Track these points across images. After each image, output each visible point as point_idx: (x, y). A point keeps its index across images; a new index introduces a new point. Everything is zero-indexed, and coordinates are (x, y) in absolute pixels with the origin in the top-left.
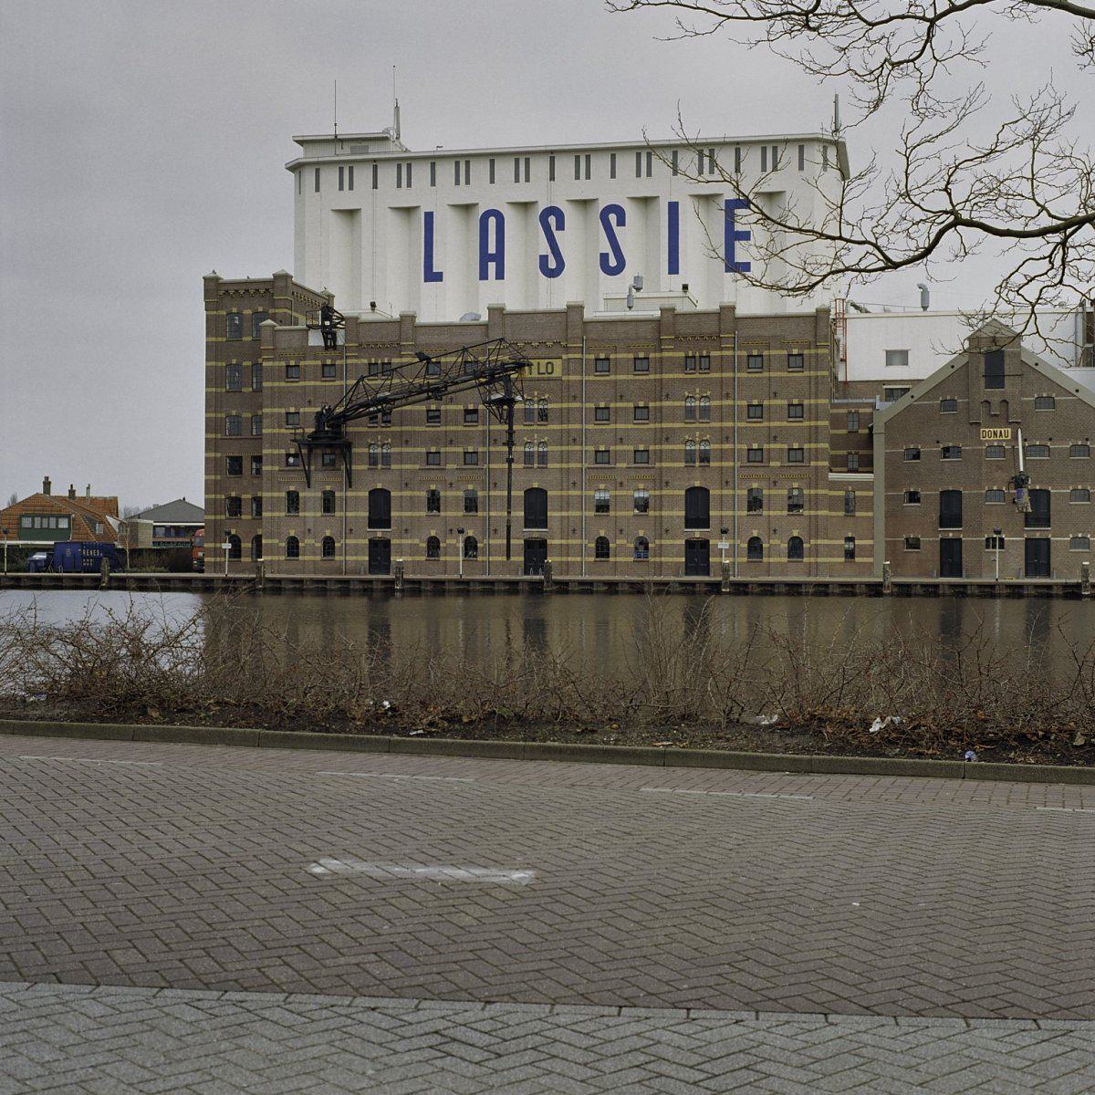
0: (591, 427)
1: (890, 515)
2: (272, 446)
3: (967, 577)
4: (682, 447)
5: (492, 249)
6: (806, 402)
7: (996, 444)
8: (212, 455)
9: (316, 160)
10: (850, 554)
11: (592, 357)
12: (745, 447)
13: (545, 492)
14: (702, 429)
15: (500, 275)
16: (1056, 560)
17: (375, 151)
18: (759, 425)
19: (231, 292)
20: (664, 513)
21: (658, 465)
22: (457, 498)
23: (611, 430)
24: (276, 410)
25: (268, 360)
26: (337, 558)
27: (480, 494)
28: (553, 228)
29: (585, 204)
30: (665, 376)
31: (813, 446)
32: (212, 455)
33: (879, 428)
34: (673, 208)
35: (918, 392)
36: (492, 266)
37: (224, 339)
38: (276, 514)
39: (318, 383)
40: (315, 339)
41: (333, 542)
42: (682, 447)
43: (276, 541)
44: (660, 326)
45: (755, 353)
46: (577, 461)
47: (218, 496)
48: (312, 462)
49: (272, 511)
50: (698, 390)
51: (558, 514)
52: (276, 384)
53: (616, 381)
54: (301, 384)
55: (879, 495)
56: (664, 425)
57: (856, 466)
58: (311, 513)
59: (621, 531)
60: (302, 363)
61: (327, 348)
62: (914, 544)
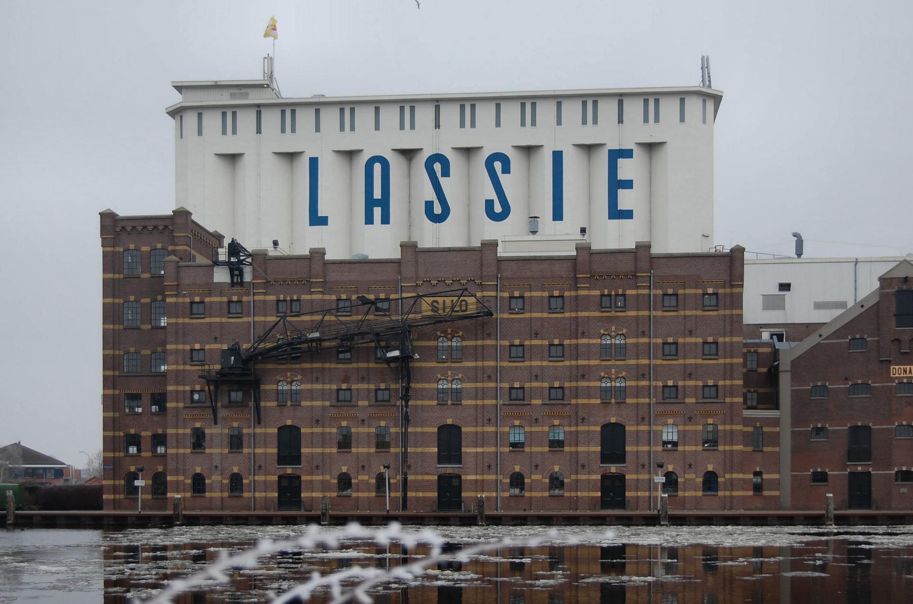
0: (505, 364)
1: (796, 450)
2: (177, 383)
3: (877, 509)
4: (598, 384)
5: (377, 194)
6: (721, 340)
7: (905, 381)
8: (110, 392)
9: (199, 104)
10: (758, 488)
11: (506, 295)
12: (660, 384)
13: (458, 429)
14: (617, 366)
15: (385, 220)
16: (877, 491)
17: (255, 97)
18: (674, 362)
19: (129, 229)
20: (580, 449)
21: (573, 401)
22: (696, 432)
23: (526, 367)
24: (181, 347)
25: (172, 296)
26: (246, 495)
27: (245, 431)
28: (439, 174)
29: (468, 152)
30: (581, 314)
31: (728, 382)
32: (110, 392)
33: (785, 363)
34: (558, 157)
35: (826, 332)
36: (377, 211)
37: (122, 276)
38: (181, 451)
39: (224, 320)
40: (221, 276)
41: (204, 479)
42: (598, 384)
43: (181, 478)
44: (575, 264)
45: (670, 291)
46: (491, 398)
47: (117, 434)
48: (219, 398)
49: (177, 448)
50: (613, 328)
51: (473, 450)
52: (180, 321)
53: (531, 319)
54: (207, 320)
55: (786, 432)
56: (580, 362)
57: (755, 403)
58: (216, 451)
59: (537, 466)
60: (207, 300)
61: (233, 284)
62: (820, 477)
